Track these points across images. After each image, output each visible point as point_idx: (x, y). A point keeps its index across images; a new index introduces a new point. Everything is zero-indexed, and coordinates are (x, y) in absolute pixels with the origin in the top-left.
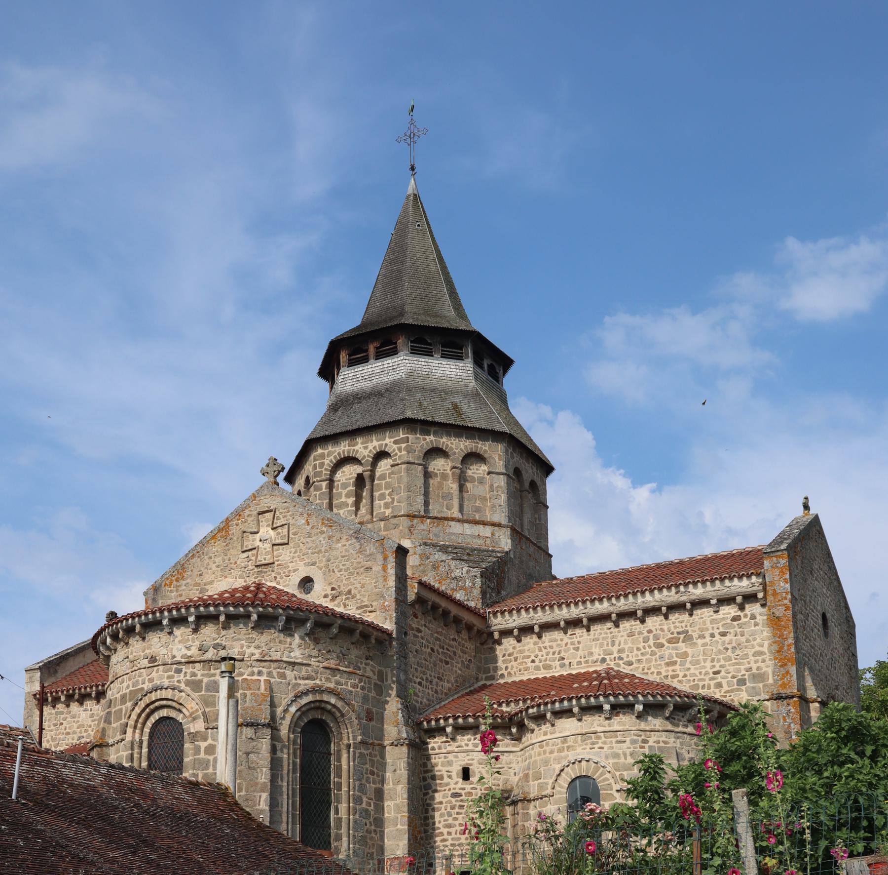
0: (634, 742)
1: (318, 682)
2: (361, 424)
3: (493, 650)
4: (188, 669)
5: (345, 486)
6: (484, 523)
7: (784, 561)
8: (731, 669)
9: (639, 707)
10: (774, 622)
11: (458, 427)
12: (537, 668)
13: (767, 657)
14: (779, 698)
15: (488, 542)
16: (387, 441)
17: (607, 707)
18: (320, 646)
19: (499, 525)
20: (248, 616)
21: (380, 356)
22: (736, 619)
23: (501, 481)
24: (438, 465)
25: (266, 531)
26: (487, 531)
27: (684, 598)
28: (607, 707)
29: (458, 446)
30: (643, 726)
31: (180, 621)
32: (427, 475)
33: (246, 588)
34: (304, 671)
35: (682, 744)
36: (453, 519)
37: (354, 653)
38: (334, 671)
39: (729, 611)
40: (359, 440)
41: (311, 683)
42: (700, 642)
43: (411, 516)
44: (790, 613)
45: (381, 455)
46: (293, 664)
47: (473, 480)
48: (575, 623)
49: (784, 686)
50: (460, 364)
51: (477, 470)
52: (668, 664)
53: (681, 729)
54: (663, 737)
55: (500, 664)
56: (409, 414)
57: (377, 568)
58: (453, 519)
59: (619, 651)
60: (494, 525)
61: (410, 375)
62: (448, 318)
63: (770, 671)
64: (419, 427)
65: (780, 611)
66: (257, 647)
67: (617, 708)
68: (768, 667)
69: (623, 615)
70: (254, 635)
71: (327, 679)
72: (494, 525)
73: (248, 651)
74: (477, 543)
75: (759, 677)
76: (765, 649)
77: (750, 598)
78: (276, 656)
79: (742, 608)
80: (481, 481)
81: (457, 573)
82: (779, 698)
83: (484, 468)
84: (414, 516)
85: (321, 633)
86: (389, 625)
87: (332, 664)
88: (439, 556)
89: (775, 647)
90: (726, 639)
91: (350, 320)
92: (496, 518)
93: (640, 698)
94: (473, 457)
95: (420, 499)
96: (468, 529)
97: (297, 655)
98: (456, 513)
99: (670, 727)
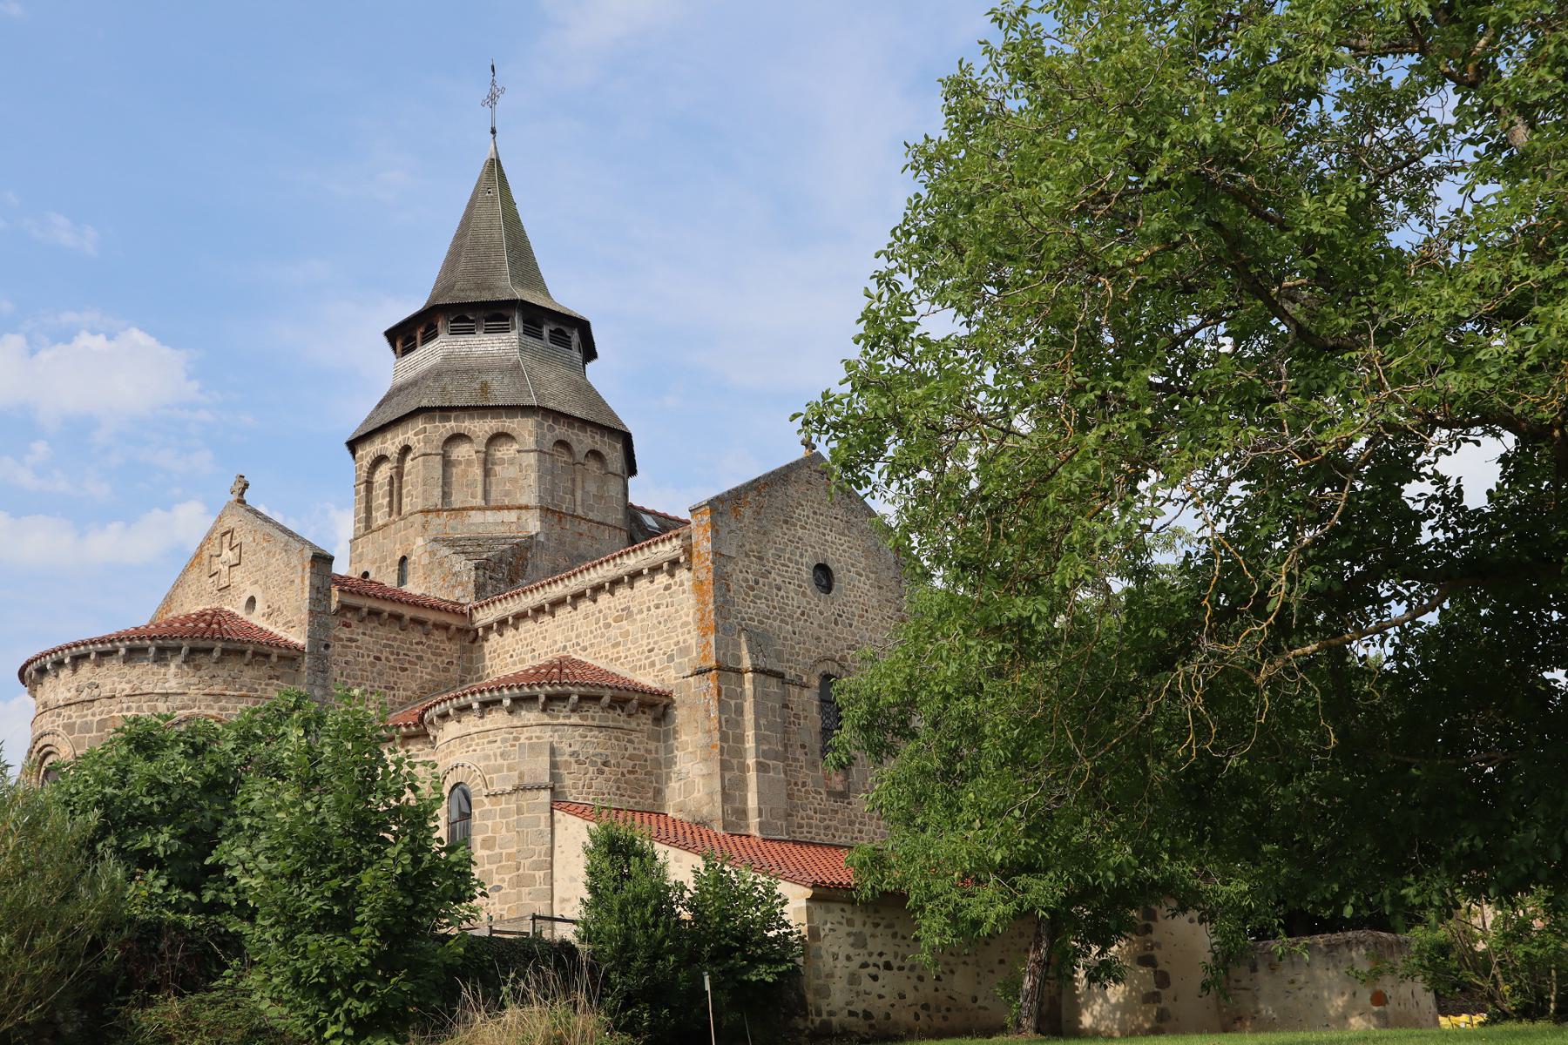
0: (504, 741)
1: (195, 710)
2: (387, 420)
3: (481, 647)
4: (65, 712)
5: (381, 487)
6: (509, 508)
7: (707, 518)
8: (663, 644)
9: (507, 702)
10: (698, 585)
11: (483, 408)
12: (514, 664)
13: (692, 627)
14: (699, 672)
15: (514, 527)
16: (410, 433)
17: (476, 705)
18: (202, 673)
19: (527, 508)
20: (116, 651)
21: (425, 340)
22: (667, 588)
23: (532, 459)
24: (461, 452)
25: (228, 555)
26: (512, 516)
27: (621, 572)
28: (476, 705)
29: (481, 428)
30: (516, 721)
31: (59, 664)
32: (447, 463)
33: (202, 615)
34: (178, 701)
35: (561, 737)
36: (473, 509)
37: (249, 674)
38: (217, 697)
39: (662, 579)
40: (389, 436)
41: (186, 712)
42: (639, 617)
43: (426, 512)
44: (711, 576)
45: (406, 450)
46: (166, 695)
47: (502, 461)
48: (539, 611)
49: (705, 658)
50: (504, 336)
51: (505, 451)
52: (614, 646)
53: (561, 721)
54: (537, 731)
55: (488, 663)
56: (425, 403)
57: (298, 581)
58: (473, 509)
59: (578, 636)
60: (520, 508)
61: (445, 358)
62: (506, 288)
63: (694, 642)
64: (438, 414)
65: (703, 575)
66: (129, 682)
67: (486, 705)
68: (692, 639)
69: (578, 596)
70: (126, 669)
71: (208, 707)
72: (520, 508)
73: (119, 687)
74: (500, 531)
75: (685, 651)
76: (690, 619)
77: (674, 563)
78: (146, 688)
79: (672, 576)
80: (512, 462)
81: (457, 568)
82: (699, 672)
83: (516, 446)
84: (429, 511)
85: (200, 658)
86: (298, 638)
87: (217, 689)
88: (445, 551)
89: (699, 616)
90: (660, 611)
91: (414, 304)
92: (523, 501)
93: (506, 691)
94: (498, 437)
95: (438, 492)
96: (490, 516)
97: (172, 685)
98: (480, 502)
99: (547, 720)
